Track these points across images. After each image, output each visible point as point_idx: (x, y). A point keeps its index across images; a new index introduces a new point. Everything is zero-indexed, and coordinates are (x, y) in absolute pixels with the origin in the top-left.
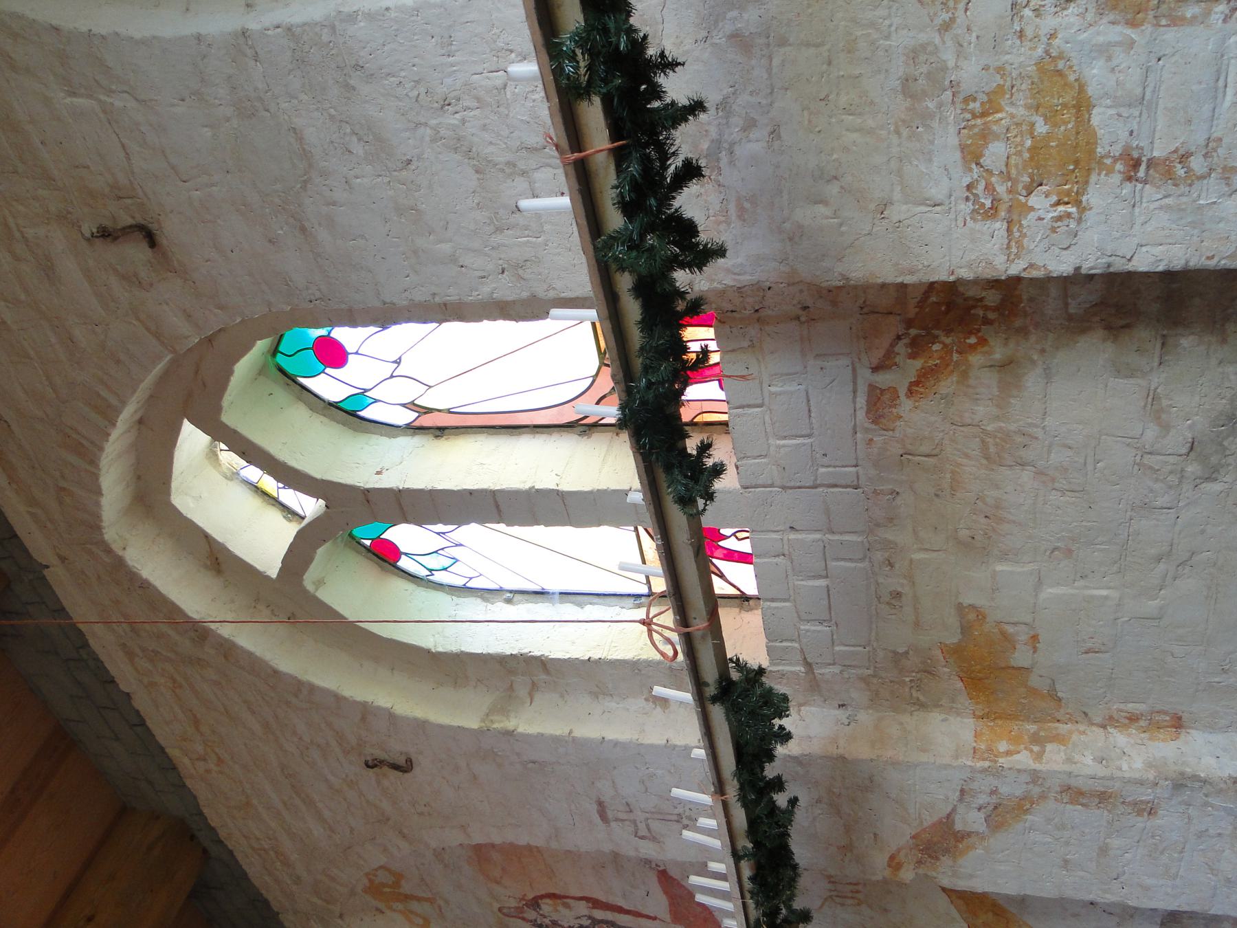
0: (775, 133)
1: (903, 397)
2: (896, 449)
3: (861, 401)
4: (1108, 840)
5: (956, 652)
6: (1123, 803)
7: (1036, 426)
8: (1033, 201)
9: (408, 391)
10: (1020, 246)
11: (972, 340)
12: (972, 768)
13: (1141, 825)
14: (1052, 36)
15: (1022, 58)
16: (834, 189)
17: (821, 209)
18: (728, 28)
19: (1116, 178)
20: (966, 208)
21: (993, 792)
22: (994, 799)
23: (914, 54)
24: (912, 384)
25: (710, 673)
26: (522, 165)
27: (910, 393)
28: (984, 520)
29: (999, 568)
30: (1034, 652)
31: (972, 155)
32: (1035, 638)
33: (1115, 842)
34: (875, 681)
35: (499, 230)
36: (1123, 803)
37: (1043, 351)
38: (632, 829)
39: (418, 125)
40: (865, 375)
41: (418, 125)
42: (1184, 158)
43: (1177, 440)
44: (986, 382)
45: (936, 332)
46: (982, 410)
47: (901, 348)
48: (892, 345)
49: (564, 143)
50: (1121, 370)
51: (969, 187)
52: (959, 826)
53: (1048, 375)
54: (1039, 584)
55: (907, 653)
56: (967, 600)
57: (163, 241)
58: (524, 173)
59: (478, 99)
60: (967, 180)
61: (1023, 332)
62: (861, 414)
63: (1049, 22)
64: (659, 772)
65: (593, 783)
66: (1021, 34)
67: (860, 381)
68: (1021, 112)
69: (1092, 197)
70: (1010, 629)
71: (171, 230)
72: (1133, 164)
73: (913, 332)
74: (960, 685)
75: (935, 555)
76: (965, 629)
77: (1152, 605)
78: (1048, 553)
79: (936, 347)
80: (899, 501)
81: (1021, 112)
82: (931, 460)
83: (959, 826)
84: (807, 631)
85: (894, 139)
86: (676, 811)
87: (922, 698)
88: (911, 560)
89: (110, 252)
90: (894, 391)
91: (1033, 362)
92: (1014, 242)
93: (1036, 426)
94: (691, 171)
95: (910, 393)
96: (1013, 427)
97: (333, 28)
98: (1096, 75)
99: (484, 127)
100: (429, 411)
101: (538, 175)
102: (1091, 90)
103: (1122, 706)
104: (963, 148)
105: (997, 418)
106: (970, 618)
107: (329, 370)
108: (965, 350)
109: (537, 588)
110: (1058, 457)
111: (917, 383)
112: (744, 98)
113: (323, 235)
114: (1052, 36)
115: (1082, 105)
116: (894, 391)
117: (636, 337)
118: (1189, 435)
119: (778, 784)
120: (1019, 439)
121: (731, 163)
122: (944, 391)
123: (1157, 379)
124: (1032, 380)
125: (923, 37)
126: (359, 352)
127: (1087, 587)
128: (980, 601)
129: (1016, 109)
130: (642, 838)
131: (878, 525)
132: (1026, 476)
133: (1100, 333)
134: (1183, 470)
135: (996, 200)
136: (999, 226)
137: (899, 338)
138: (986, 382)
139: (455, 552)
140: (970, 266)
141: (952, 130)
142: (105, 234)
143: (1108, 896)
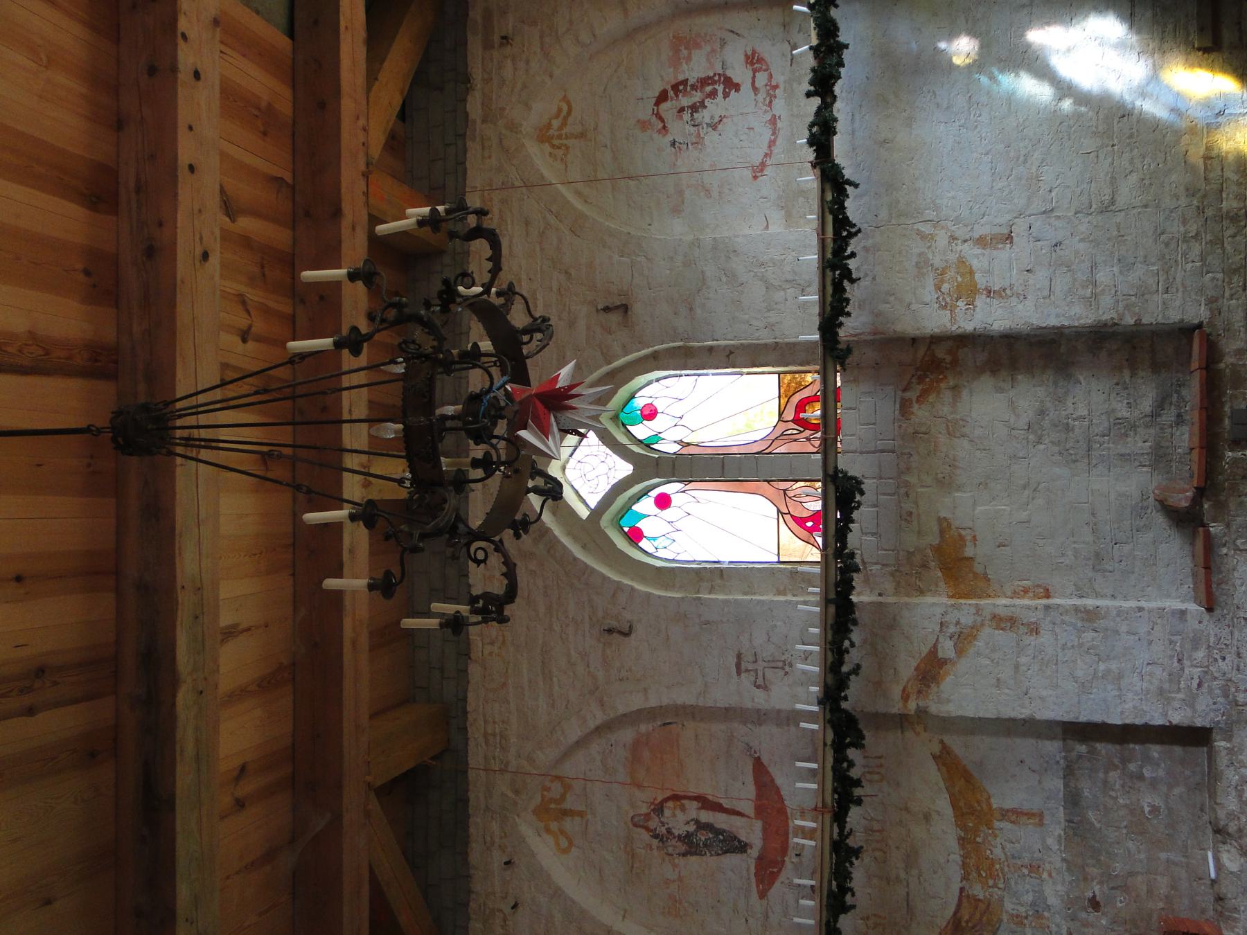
0: (874, 279)
1: (914, 404)
2: (911, 430)
3: (898, 406)
5: (938, 550)
7: (967, 416)
8: (958, 304)
9: (680, 434)
10: (955, 320)
11: (941, 377)
12: (947, 606)
14: (961, 251)
15: (953, 257)
16: (892, 298)
17: (888, 306)
18: (862, 244)
19: (984, 296)
20: (936, 306)
21: (958, 623)
22: (958, 629)
23: (920, 255)
24: (918, 397)
25: (831, 472)
26: (783, 286)
27: (918, 401)
28: (948, 468)
29: (956, 495)
30: (975, 546)
31: (938, 288)
32: (974, 538)
33: (1023, 660)
34: (898, 574)
35: (769, 311)
37: (968, 381)
39: (750, 271)
40: (900, 393)
41: (750, 271)
42: (1004, 290)
43: (1022, 423)
44: (947, 396)
45: (928, 373)
46: (946, 410)
47: (914, 380)
48: (911, 379)
49: (821, 233)
50: (1000, 390)
51: (937, 298)
52: (940, 655)
53: (971, 392)
54: (975, 504)
55: (914, 552)
56: (943, 514)
57: (630, 313)
58: (784, 289)
59: (774, 263)
60: (936, 296)
61: (961, 373)
62: (897, 412)
63: (959, 248)
64: (779, 623)
66: (952, 250)
67: (898, 397)
68: (952, 274)
69: (978, 303)
70: (963, 532)
71: (637, 308)
72: (989, 292)
73: (919, 373)
74: (940, 574)
75: (927, 489)
76: (942, 532)
77: (1024, 515)
79: (928, 380)
80: (912, 459)
81: (952, 274)
82: (926, 436)
84: (866, 540)
85: (913, 282)
86: (783, 658)
88: (917, 493)
89: (603, 317)
90: (910, 400)
91: (964, 386)
92: (953, 319)
93: (967, 416)
94: (853, 255)
95: (918, 401)
96: (958, 417)
97: (730, 238)
98: (975, 264)
99: (773, 273)
100: (688, 444)
101: (788, 291)
102: (974, 268)
104: (935, 285)
105: (952, 413)
106: (944, 525)
107: (645, 422)
108: (939, 381)
109: (716, 560)
110: (978, 432)
111: (920, 396)
112: (865, 267)
113: (699, 311)
114: (961, 251)
115: (972, 273)
116: (910, 400)
117: (829, 299)
118: (1027, 420)
119: (853, 521)
120: (961, 423)
121: (858, 288)
122: (931, 400)
123: (1011, 393)
124: (965, 393)
125: (922, 250)
126: (665, 412)
127: (996, 505)
128: (949, 516)
129: (951, 273)
130: (758, 687)
131: (902, 473)
132: (965, 443)
133: (988, 373)
134: (1027, 438)
135: (946, 303)
136: (948, 312)
137: (913, 376)
138: (947, 396)
139: (675, 535)
140: (938, 327)
141: (932, 280)
142: (607, 309)
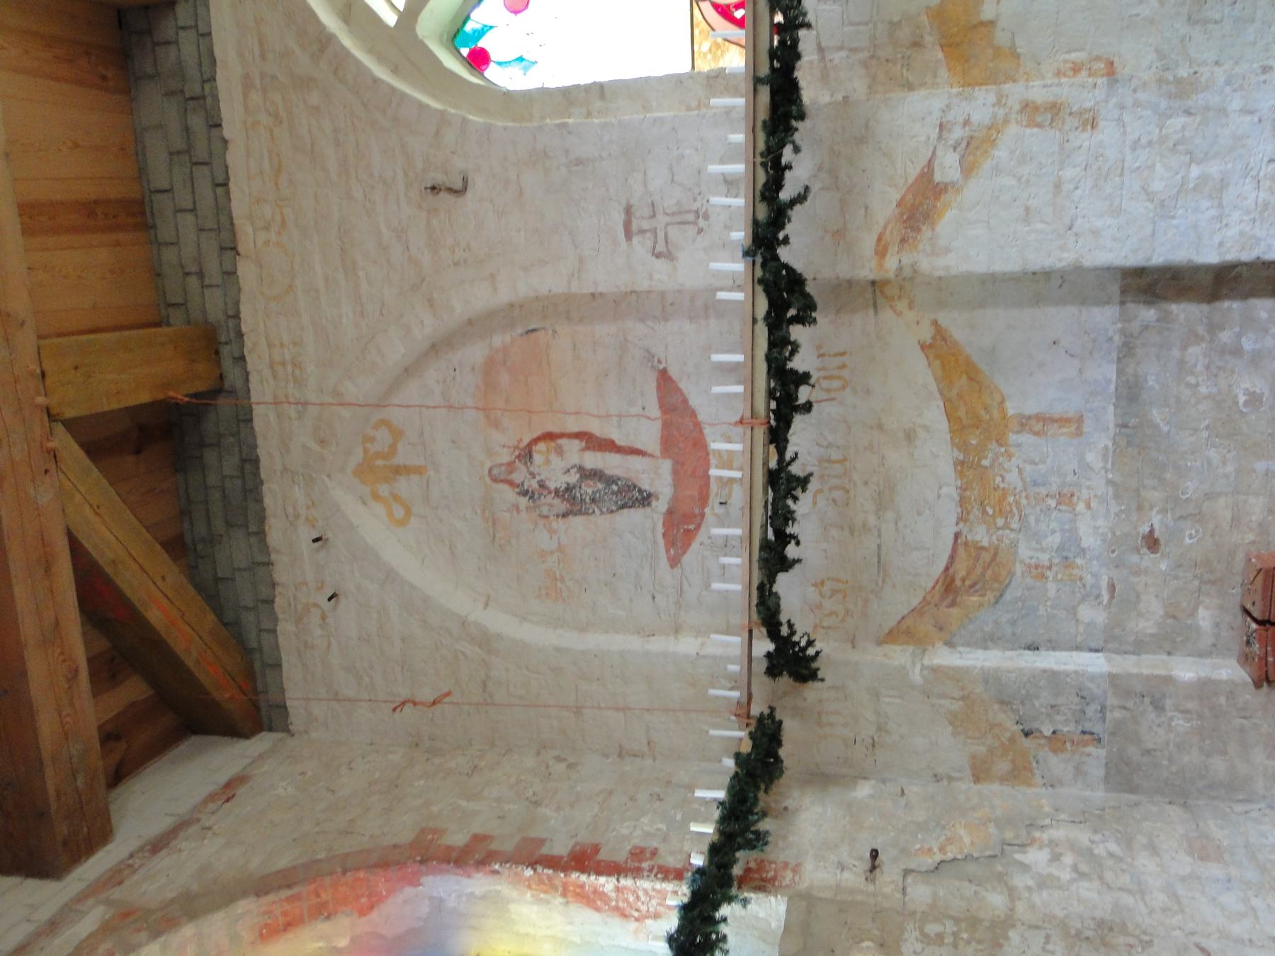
4: (1061, 173)
6: (1071, 114)
13: (1086, 144)
21: (967, 122)
22: (966, 132)
36: (1071, 114)
38: (650, 244)
55: (900, 22)
64: (688, 152)
65: (626, 180)
74: (940, 55)
78: (1033, 196)
83: (938, 177)
87: (911, 79)
103: (1067, 57)
143: (1065, 255)
